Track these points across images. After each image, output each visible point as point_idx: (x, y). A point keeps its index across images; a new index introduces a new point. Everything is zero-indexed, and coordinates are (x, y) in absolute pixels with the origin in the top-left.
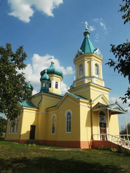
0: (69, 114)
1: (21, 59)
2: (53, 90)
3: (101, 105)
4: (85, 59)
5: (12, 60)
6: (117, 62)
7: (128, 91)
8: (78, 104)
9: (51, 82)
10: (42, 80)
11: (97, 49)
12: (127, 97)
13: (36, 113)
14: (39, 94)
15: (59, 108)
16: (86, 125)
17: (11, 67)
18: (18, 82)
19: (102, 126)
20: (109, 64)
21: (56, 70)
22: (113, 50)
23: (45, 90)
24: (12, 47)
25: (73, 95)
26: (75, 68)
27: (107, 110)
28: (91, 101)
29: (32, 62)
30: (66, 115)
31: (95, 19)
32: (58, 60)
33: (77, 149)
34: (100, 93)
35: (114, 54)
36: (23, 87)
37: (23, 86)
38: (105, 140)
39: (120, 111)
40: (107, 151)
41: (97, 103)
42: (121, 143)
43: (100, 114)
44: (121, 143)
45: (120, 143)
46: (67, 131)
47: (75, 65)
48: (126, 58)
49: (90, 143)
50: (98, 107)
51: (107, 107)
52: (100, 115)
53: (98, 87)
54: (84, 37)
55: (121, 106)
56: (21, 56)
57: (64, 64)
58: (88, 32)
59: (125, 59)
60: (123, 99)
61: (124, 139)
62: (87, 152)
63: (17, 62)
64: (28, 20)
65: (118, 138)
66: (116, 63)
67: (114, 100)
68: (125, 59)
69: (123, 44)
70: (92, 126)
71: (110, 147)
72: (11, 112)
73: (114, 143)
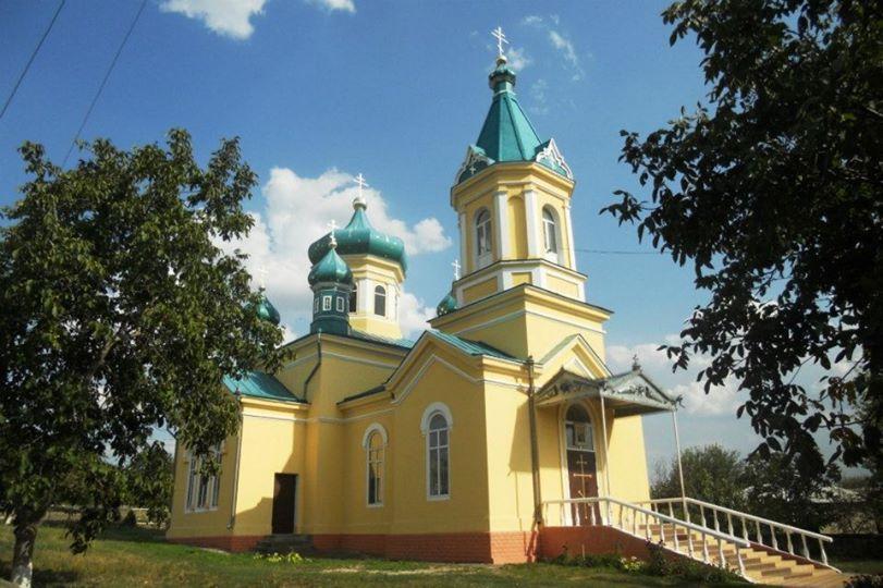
0: (438, 420)
1: (231, 194)
2: (364, 320)
3: (572, 379)
4: (501, 189)
5: (194, 201)
6: (648, 203)
7: (693, 321)
8: (475, 380)
9: (355, 288)
10: (319, 280)
11: (546, 144)
12: (688, 345)
13: (296, 423)
14: (308, 341)
15: (393, 397)
16: (510, 465)
17: (193, 231)
18: (220, 294)
19: (579, 465)
20: (617, 211)
21: (375, 237)
22: (632, 154)
23: (331, 325)
24: (194, 144)
25: (451, 338)
26: (459, 225)
27: (598, 398)
28: (529, 363)
29: (268, 206)
30: (425, 425)
31: (528, 16)
32: (379, 193)
33: (478, 565)
34: (563, 327)
35: (635, 171)
36: (242, 316)
37: (244, 311)
38: (594, 524)
39: (652, 403)
40: (604, 569)
41: (555, 371)
42: (659, 533)
43: (568, 419)
44: (659, 533)
45: (654, 533)
46: (434, 492)
47: (457, 214)
48: (684, 184)
49: (532, 539)
50: (558, 385)
51: (598, 389)
52: (571, 423)
53: (558, 303)
54: (492, 94)
55: (653, 382)
56: (230, 182)
57: (406, 208)
58: (506, 73)
59: (682, 192)
60: (673, 353)
61: (672, 517)
62: (519, 576)
63: (217, 207)
64: (243, 29)
65: (647, 514)
66: (645, 205)
67: (622, 358)
68: (682, 192)
69: (670, 128)
70: (535, 469)
71: (613, 552)
72: (199, 420)
73: (627, 535)
